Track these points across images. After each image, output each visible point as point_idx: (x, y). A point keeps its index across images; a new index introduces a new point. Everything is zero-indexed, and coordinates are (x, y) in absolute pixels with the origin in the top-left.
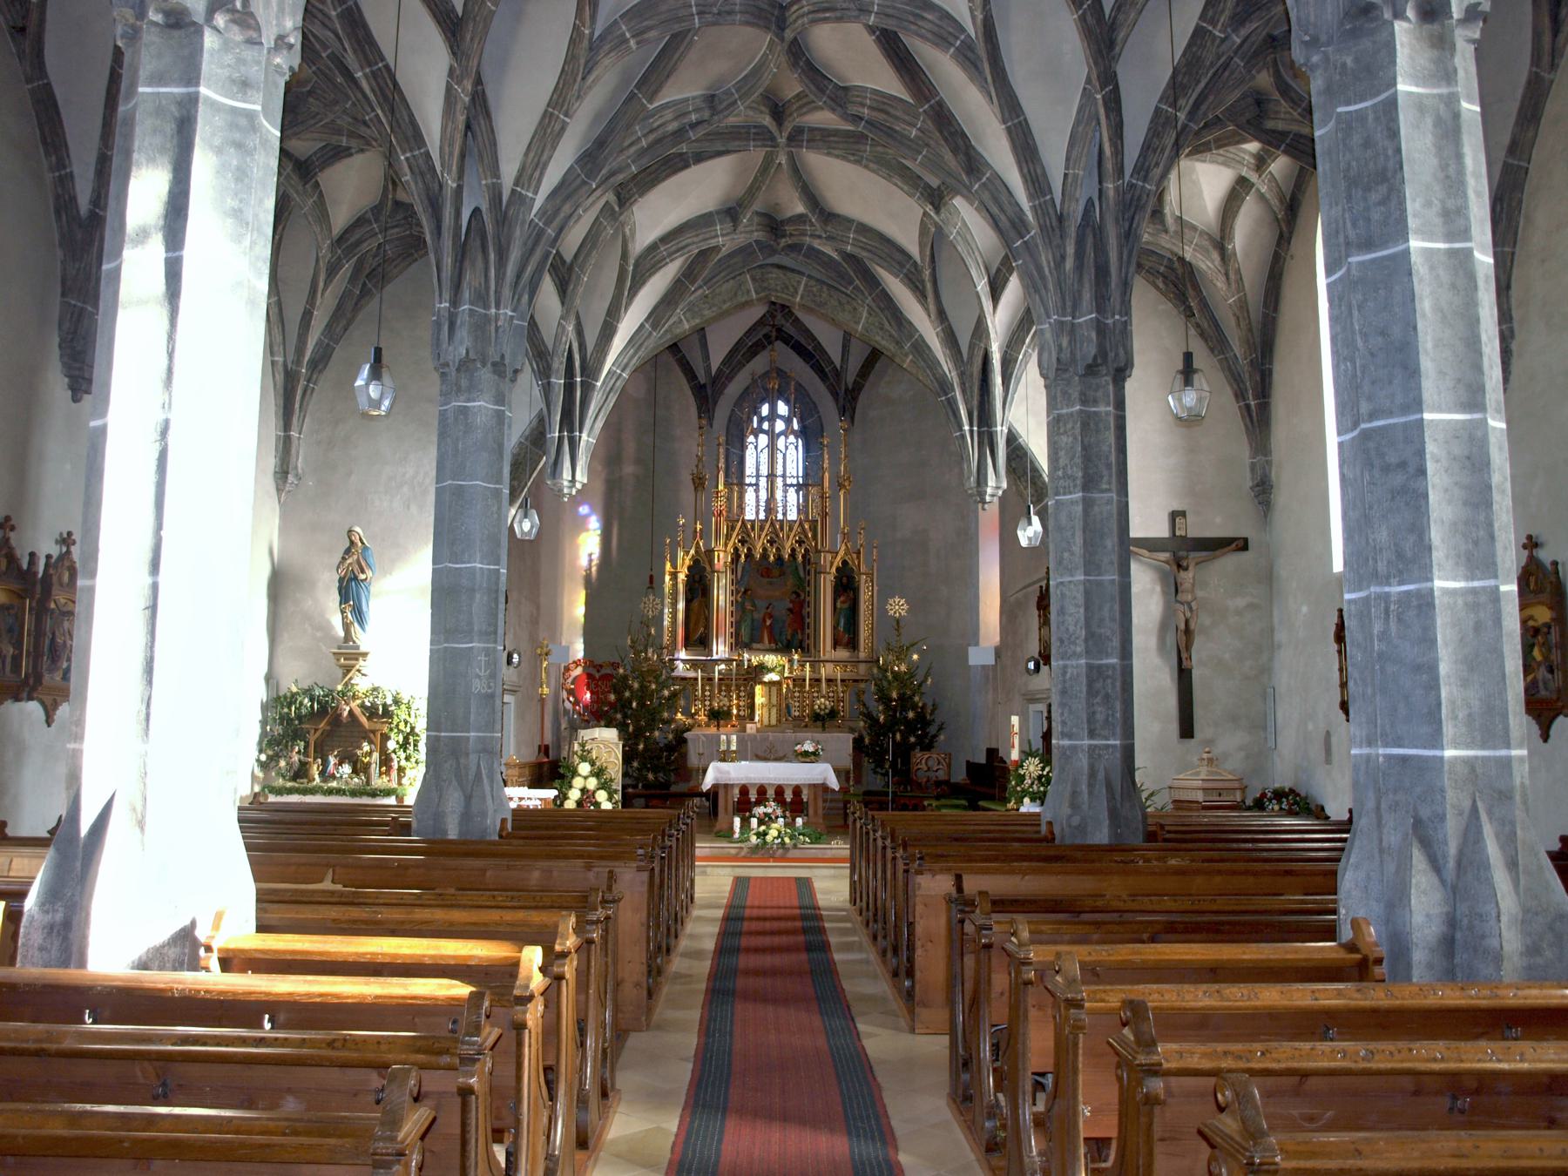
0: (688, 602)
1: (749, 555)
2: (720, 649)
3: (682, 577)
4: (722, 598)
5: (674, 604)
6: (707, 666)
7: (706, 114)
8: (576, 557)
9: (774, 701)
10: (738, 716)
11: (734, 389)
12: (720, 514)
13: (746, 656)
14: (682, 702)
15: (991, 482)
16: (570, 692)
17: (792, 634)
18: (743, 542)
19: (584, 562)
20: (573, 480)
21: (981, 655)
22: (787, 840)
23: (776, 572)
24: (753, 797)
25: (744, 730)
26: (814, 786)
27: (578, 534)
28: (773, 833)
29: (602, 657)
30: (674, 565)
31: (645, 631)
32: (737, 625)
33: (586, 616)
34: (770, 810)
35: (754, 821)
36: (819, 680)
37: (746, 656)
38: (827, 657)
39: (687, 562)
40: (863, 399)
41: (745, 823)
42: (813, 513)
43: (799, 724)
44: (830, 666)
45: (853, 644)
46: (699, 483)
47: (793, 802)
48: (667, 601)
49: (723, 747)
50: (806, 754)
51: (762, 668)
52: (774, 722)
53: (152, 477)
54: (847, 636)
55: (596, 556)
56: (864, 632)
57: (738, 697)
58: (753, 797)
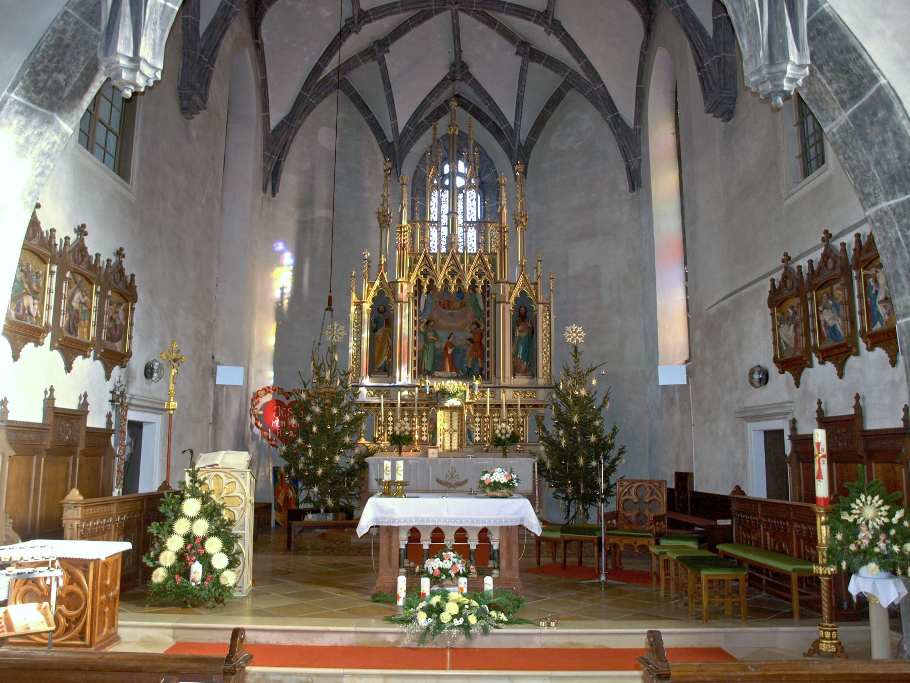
0: (373, 331)
1: (432, 286)
2: (404, 376)
3: (367, 306)
4: (405, 326)
5: (359, 332)
6: (388, 392)
7: (450, 340)
8: (270, 290)
9: (455, 426)
10: (420, 441)
11: (419, 147)
12: (403, 247)
13: (428, 381)
14: (364, 427)
15: (793, 55)
16: (258, 418)
17: (473, 362)
18: (425, 274)
19: (277, 295)
20: (135, 59)
21: (672, 374)
22: (472, 619)
23: (457, 304)
24: (426, 544)
25: (426, 454)
26: (506, 530)
27: (273, 270)
28: (452, 608)
29: (293, 385)
30: (360, 296)
31: (326, 359)
32: (420, 354)
33: (276, 345)
34: (447, 565)
35: (425, 582)
36: (499, 406)
37: (428, 381)
38: (507, 383)
39: (372, 293)
40: (534, 153)
41: (413, 588)
42: (493, 247)
43: (480, 449)
44: (509, 392)
45: (531, 371)
46: (384, 220)
47: (478, 550)
48: (352, 330)
49: (387, 478)
50: (496, 485)
52: (455, 447)
54: (526, 363)
55: (288, 290)
56: (542, 360)
57: (420, 423)
58: (426, 544)
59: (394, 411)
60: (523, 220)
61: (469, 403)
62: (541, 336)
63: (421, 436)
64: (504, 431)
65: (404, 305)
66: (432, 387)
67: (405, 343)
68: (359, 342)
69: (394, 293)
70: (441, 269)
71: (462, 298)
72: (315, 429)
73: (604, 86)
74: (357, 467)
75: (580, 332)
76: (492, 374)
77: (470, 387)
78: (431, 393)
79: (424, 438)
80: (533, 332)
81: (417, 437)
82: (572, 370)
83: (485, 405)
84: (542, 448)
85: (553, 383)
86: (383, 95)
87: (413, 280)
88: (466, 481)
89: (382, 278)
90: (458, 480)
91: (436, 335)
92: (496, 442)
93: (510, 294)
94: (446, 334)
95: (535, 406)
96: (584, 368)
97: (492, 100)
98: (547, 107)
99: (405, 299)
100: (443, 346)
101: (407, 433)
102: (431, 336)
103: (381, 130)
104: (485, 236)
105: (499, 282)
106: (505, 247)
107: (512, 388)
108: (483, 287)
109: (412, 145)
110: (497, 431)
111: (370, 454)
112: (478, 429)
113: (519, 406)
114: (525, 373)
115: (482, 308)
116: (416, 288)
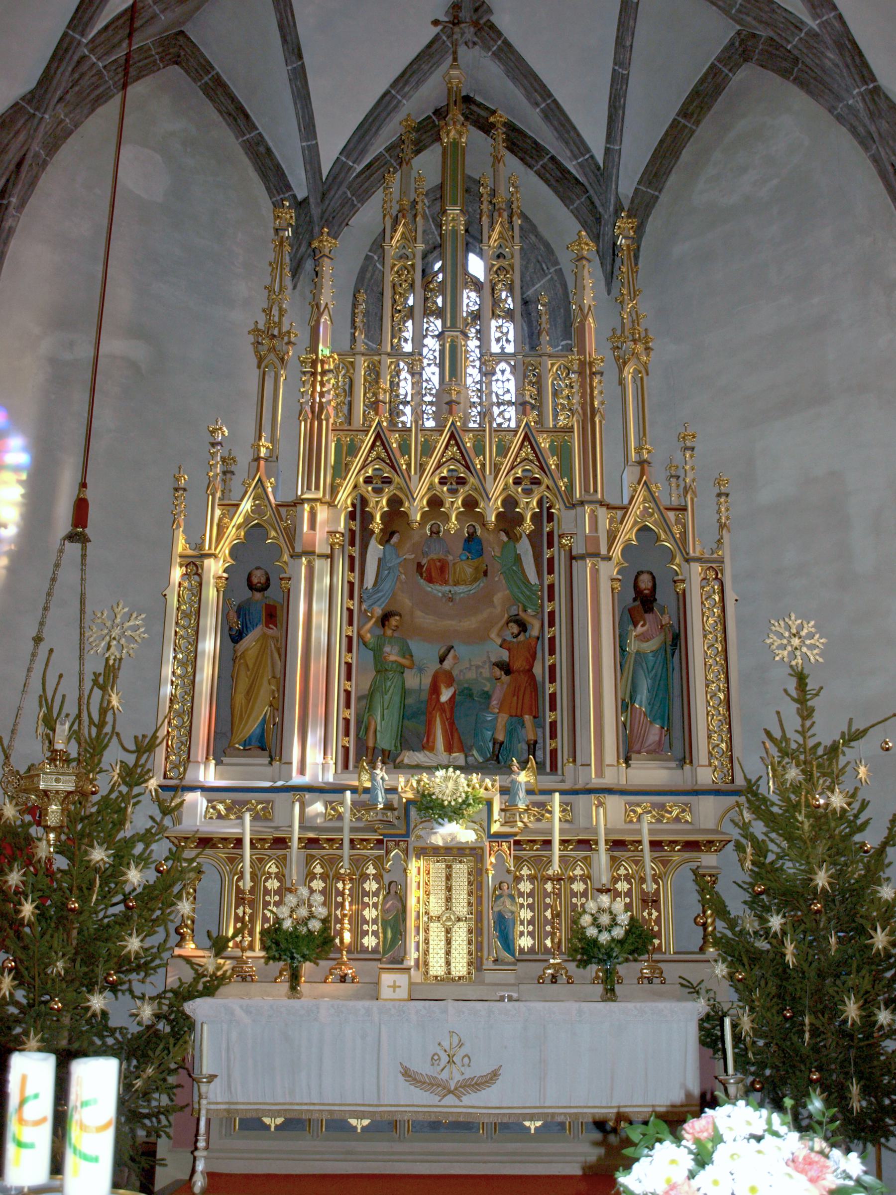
0: (233, 636)
1: (396, 513)
2: (313, 758)
3: (215, 568)
4: (320, 620)
9: (461, 906)
17: (506, 712)
38: (610, 778)
39: (231, 532)
44: (615, 804)
51: (431, 808)
52: (460, 967)
53: (686, 964)
54: (660, 712)
59: (283, 861)
60: (640, 348)
61: (498, 835)
62: (699, 647)
63: (359, 934)
64: (605, 919)
65: (318, 563)
66: (393, 790)
67: (318, 666)
68: (191, 662)
69: (291, 534)
70: (422, 468)
71: (480, 553)
72: (28, 909)
73: (840, 17)
74: (163, 1027)
75: (811, 636)
76: (563, 755)
77: (504, 791)
78: (389, 807)
79: (370, 942)
80: (677, 641)
81: (347, 937)
82: (795, 738)
83: (548, 843)
84: (721, 969)
85: (740, 781)
86: (280, 72)
87: (344, 497)
88: (494, 1076)
89: (261, 496)
90: (469, 1073)
91: (406, 652)
92: (584, 951)
93: (612, 538)
94: (436, 650)
95: (692, 846)
96: (825, 732)
97: (550, 95)
98: (684, 112)
99: (321, 547)
100: (427, 681)
101: (315, 925)
102: (392, 654)
103: (278, 167)
104: (539, 384)
105: (582, 503)
106: (594, 412)
107: (622, 792)
108: (536, 518)
109: (354, 209)
110: (586, 920)
111: (210, 986)
112: (526, 914)
113: (646, 846)
114: (656, 752)
115: (533, 578)
116: (356, 526)
